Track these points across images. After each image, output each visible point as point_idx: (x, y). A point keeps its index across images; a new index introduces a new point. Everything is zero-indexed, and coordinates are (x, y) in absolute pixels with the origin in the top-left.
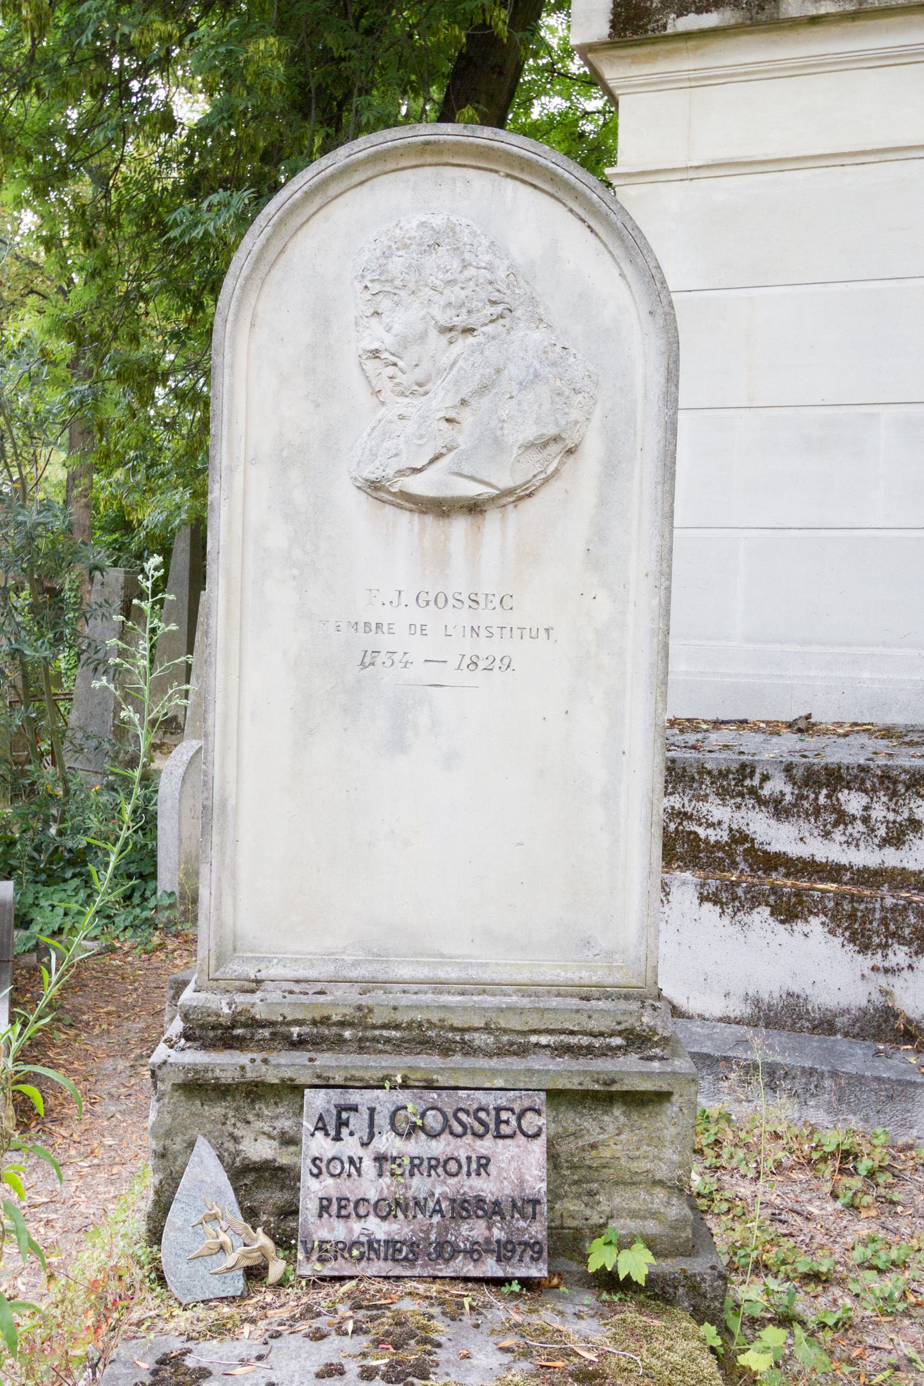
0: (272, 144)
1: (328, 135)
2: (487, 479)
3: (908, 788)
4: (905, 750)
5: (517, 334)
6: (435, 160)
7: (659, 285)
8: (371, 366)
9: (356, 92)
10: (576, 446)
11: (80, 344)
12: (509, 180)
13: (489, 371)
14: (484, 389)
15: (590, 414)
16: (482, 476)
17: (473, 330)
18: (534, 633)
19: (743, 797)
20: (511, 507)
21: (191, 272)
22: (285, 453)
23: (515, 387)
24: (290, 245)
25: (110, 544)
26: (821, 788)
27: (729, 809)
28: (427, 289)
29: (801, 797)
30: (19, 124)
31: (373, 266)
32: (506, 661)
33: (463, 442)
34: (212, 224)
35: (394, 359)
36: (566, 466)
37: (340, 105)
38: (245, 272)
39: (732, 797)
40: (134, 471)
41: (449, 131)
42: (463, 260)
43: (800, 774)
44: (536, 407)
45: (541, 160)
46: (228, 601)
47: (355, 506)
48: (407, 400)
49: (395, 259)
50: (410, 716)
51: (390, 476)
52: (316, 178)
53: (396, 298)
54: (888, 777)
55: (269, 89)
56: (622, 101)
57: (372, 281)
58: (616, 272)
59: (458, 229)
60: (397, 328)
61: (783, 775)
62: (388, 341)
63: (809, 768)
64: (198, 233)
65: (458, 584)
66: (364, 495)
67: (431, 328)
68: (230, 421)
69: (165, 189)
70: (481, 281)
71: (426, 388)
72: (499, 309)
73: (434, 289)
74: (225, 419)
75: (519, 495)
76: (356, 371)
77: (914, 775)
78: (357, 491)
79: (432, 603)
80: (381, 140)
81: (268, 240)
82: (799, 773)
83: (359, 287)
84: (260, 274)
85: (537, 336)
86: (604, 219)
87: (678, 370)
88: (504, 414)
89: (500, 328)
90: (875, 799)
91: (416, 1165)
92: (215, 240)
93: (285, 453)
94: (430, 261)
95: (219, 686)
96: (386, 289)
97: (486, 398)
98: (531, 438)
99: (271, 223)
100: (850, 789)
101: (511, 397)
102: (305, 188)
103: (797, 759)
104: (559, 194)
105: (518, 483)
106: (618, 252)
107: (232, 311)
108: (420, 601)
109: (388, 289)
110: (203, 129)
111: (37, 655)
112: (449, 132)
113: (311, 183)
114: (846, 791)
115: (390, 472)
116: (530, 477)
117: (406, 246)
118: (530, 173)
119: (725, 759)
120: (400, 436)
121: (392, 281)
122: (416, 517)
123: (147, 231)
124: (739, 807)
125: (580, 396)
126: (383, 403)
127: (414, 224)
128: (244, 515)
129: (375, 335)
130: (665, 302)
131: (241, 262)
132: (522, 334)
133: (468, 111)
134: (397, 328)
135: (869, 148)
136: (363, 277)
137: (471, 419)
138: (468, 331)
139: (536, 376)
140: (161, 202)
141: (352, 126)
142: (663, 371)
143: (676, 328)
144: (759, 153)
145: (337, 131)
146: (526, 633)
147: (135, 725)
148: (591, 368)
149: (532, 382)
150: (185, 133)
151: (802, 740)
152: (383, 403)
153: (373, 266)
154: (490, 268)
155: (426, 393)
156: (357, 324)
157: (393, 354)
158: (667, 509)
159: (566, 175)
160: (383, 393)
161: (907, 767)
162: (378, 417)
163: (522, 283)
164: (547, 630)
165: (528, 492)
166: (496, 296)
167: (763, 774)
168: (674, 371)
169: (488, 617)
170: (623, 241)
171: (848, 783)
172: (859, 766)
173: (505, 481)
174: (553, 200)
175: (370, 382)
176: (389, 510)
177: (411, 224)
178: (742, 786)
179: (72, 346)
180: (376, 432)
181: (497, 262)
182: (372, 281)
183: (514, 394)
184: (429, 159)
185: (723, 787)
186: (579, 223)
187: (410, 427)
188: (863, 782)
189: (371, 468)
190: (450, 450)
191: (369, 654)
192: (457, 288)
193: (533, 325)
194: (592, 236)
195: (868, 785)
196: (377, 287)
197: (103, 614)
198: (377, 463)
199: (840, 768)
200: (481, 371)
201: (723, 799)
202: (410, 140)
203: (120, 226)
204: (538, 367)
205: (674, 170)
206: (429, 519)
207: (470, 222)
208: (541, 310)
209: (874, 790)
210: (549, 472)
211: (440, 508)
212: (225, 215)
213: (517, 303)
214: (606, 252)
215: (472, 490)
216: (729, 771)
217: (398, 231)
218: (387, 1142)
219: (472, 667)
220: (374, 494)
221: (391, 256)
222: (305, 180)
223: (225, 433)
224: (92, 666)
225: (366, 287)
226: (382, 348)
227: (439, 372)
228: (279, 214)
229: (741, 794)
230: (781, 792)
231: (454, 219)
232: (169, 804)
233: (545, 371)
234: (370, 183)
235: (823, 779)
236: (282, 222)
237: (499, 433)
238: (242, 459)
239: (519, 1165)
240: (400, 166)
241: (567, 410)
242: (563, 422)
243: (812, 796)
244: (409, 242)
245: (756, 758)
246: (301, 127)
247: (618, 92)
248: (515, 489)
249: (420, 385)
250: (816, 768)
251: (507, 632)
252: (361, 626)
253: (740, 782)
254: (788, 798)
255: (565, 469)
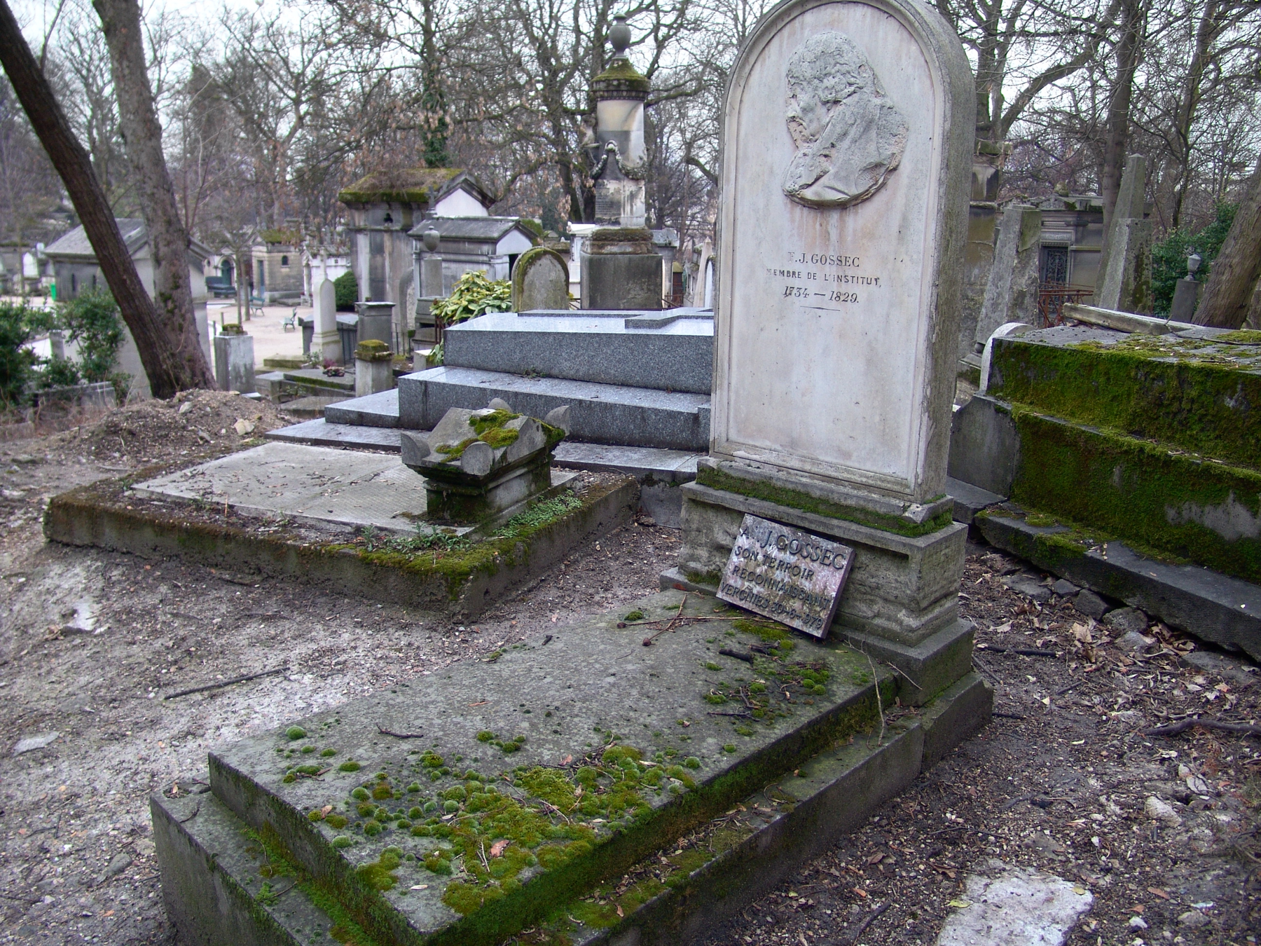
62: (799, 112)
91: (781, 564)
115: (797, 187)
138: (836, 102)
147: (1002, 399)
173: (854, 191)
218: (773, 551)
239: (828, 581)
255: (890, 182)
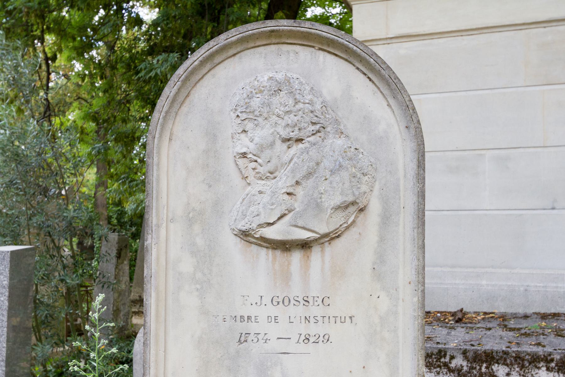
0: (188, 30)
1: (214, 26)
2: (312, 229)
3: (530, 363)
4: (524, 339)
5: (329, 141)
6: (277, 41)
7: (411, 111)
8: (242, 162)
9: (227, 6)
10: (365, 207)
11: (97, 124)
12: (321, 52)
13: (312, 164)
14: (309, 175)
15: (372, 187)
16: (310, 226)
17: (302, 140)
18: (343, 320)
19: (441, 368)
20: (327, 244)
21: (150, 90)
22: (191, 215)
23: (328, 174)
24: (192, 92)
25: (116, 211)
26: (482, 363)
27: (433, 374)
28: (274, 117)
29: (472, 368)
30: (69, 22)
31: (242, 103)
32: (326, 337)
33: (298, 206)
34: (159, 70)
35: (255, 158)
36: (359, 219)
37: (219, 12)
38: (165, 109)
39: (435, 368)
40: (124, 183)
41: (285, 24)
42: (295, 99)
43: (471, 355)
44: (341, 184)
45: (340, 40)
46: (157, 306)
47: (233, 244)
48: (263, 182)
49: (255, 99)
50: (269, 372)
51: (254, 228)
52: (207, 53)
53: (256, 122)
54: (519, 358)
55: (186, 6)
56: (354, 8)
57: (242, 112)
58: (385, 104)
59: (292, 81)
60: (257, 140)
61: (462, 356)
62: (252, 147)
63: (476, 352)
64: (152, 74)
65: (296, 291)
66: (239, 239)
67: (277, 139)
68: (157, 197)
69: (138, 52)
70: (307, 111)
71: (275, 175)
72: (317, 127)
73: (278, 116)
74: (154, 196)
75: (331, 237)
76: (232, 165)
77: (533, 356)
78: (235, 237)
79: (281, 303)
80: (245, 30)
81: (179, 89)
82: (470, 355)
83: (234, 116)
84: (174, 109)
85: (340, 142)
86: (378, 73)
87: (424, 161)
88: (322, 189)
89: (318, 138)
90: (512, 369)
92: (161, 77)
93: (191, 215)
94: (275, 100)
95: (152, 359)
96: (250, 117)
97: (310, 180)
98: (339, 204)
99: (181, 79)
100: (498, 364)
101: (326, 179)
102: (200, 59)
103: (468, 347)
104: (351, 59)
105: (331, 230)
106: (386, 92)
107: (157, 132)
108: (274, 302)
109: (251, 117)
110: (155, 24)
111: (73, 282)
112: (271, 25)
113: (204, 55)
114: (497, 365)
115: (254, 226)
116: (338, 226)
117: (261, 92)
118: (333, 47)
119: (430, 347)
120: (260, 203)
121: (253, 112)
122: (270, 251)
123: (130, 71)
124: (438, 373)
125: (366, 177)
126: (249, 184)
127: (266, 79)
128: (166, 252)
129: (244, 144)
130: (415, 121)
131: (169, 91)
132: (331, 141)
133: (280, 14)
134: (257, 140)
135: (474, 27)
136: (236, 110)
137: (302, 193)
138: (299, 140)
139: (341, 166)
140: (136, 58)
141: (225, 22)
142: (415, 161)
143: (422, 136)
144: (421, 30)
145: (218, 24)
146: (338, 320)
148: (372, 160)
149: (338, 170)
150: (147, 26)
151: (468, 333)
152: (249, 184)
153: (242, 103)
154: (311, 103)
155: (275, 178)
156: (233, 138)
157: (255, 155)
158: (420, 243)
159: (355, 48)
160: (249, 178)
161: (529, 352)
162: (246, 192)
163: (330, 111)
164: (351, 317)
165: (337, 235)
166: (315, 120)
167: (450, 355)
168: (422, 161)
169: (315, 310)
170: (389, 86)
171: (497, 360)
172: (503, 351)
173: (323, 229)
174: (347, 63)
175: (241, 172)
176: (254, 247)
177: (264, 78)
178: (440, 362)
179: (94, 124)
180: (245, 201)
181: (315, 99)
182: (242, 112)
183: (327, 177)
184: (274, 41)
185: (429, 362)
186: (362, 76)
187: (266, 198)
188: (505, 360)
189: (243, 223)
190: (290, 212)
191: (243, 335)
192: (292, 116)
193: (337, 136)
194: (371, 83)
195: (508, 361)
196: (244, 116)
197: (107, 260)
198: (246, 220)
199: (492, 352)
200: (308, 164)
201: (430, 369)
202: (262, 29)
203: (117, 69)
204: (341, 160)
205: (380, 39)
206: (278, 253)
207: (299, 77)
208: (342, 127)
209: (512, 364)
210: (349, 222)
211: (285, 246)
212: (165, 66)
213: (328, 123)
214: (379, 92)
215: (304, 235)
216: (432, 354)
217: (256, 82)
219: (306, 341)
220: (245, 239)
221: (252, 97)
222: (200, 54)
223: (154, 204)
224: (102, 285)
225: (238, 116)
226: (248, 151)
227: (282, 165)
228: (185, 74)
229: (440, 366)
230: (461, 365)
231: (289, 75)
232: (139, 357)
233: (346, 163)
234: (239, 55)
235: (484, 359)
236: (187, 79)
237: (319, 201)
238: (165, 219)
240: (256, 45)
241: (359, 186)
242: (357, 193)
243: (478, 368)
244: (263, 89)
245: (447, 346)
246: (201, 23)
247: (352, 3)
248: (329, 233)
249: (271, 173)
250: (479, 352)
251: (326, 319)
252: (238, 318)
253: (438, 360)
254: (465, 368)
